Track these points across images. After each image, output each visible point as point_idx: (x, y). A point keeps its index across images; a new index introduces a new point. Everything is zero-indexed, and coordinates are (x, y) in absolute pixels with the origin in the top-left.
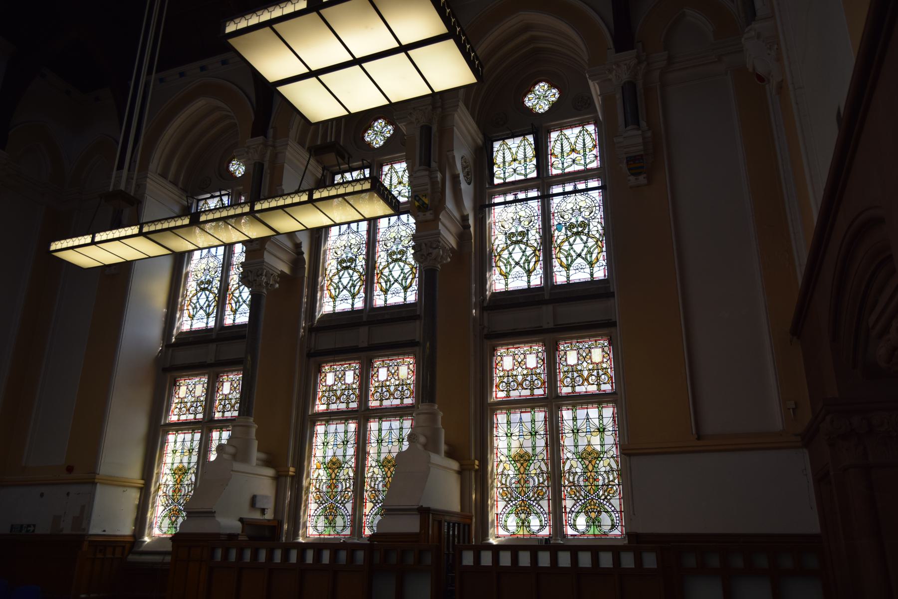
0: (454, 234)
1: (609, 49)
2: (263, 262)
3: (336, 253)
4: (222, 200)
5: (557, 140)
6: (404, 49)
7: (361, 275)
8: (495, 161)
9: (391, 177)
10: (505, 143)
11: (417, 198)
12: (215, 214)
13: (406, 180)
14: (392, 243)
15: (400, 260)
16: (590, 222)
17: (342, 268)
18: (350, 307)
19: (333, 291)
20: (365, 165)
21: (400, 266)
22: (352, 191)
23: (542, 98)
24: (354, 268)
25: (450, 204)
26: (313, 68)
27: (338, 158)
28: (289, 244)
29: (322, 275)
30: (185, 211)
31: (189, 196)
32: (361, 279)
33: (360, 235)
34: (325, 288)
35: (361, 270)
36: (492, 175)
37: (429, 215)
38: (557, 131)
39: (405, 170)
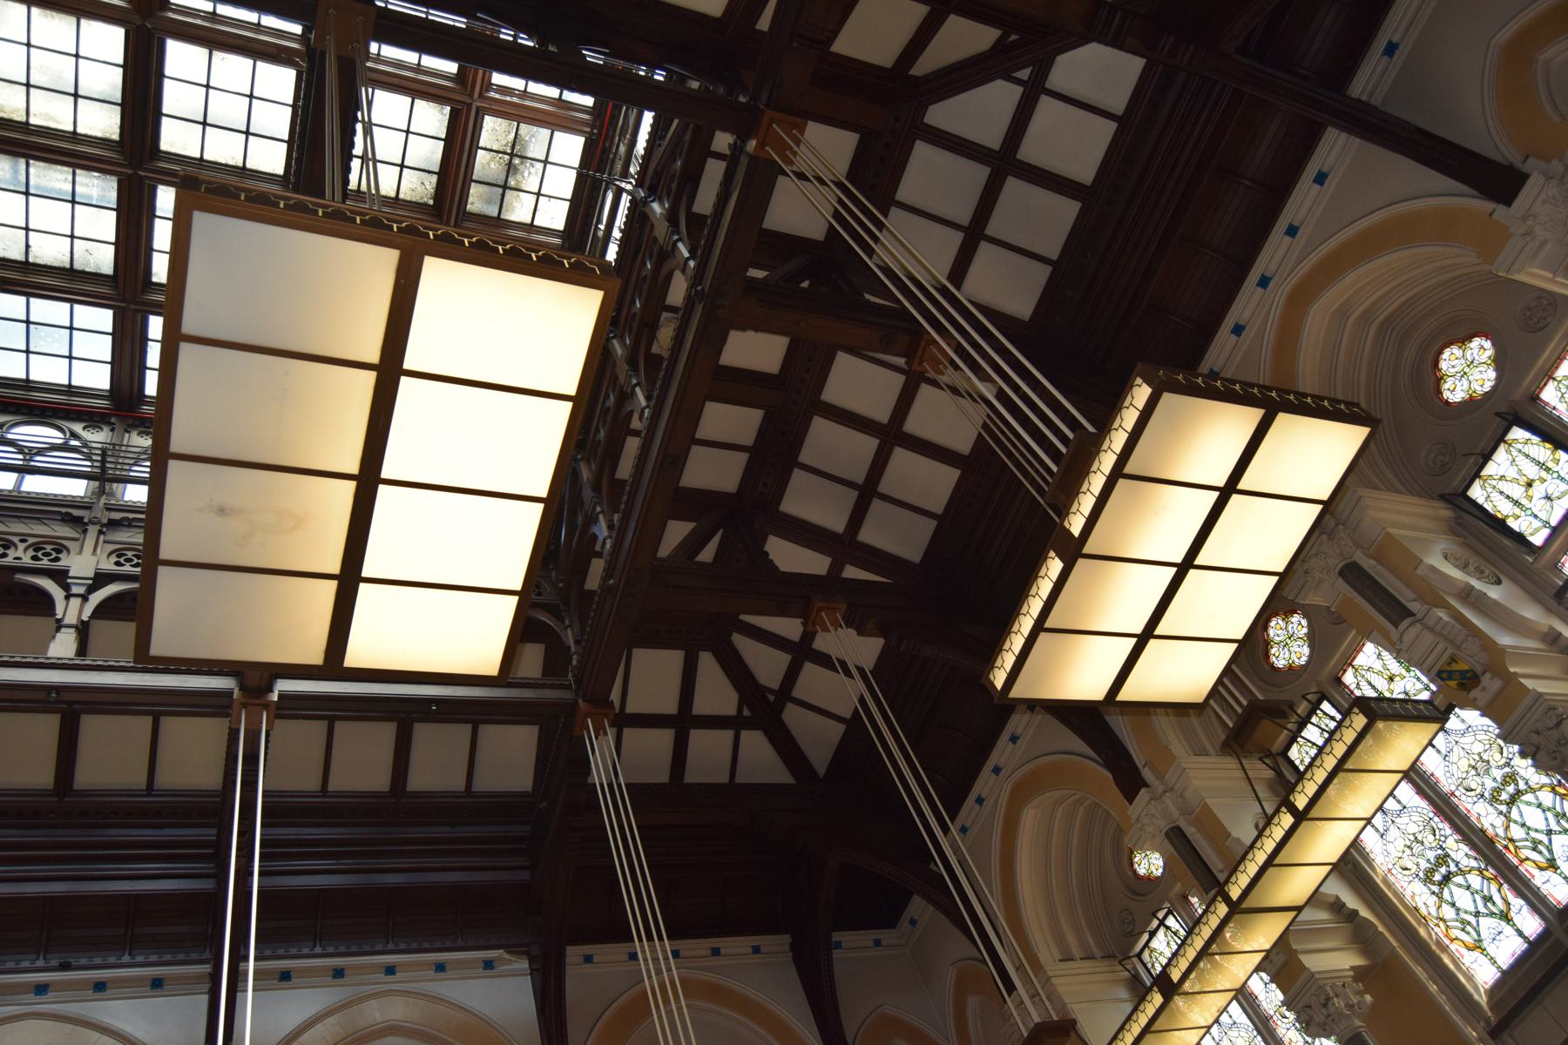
0: (1562, 676)
1: (1491, 214)
2: (1312, 975)
3: (1406, 869)
4: (1168, 928)
5: (1562, 396)
6: (1228, 491)
7: (1481, 872)
8: (1500, 516)
9: (1370, 684)
10: (1485, 478)
11: (1444, 675)
12: (1238, 882)
13: (1394, 666)
14: (1476, 778)
15: (1519, 793)
16: (1444, 849)
17: (1439, 885)
18: (1520, 940)
19: (1462, 936)
20: (1313, 701)
21: (1528, 804)
22: (1355, 735)
23: (1467, 370)
24: (1460, 869)
25: (1505, 640)
26: (1138, 630)
27: (1276, 720)
28: (1320, 915)
29: (1419, 923)
30: (1140, 994)
31: (1123, 960)
32: (1488, 879)
33: (1414, 809)
34: (1447, 942)
35: (1474, 863)
36: (1520, 538)
37: (1490, 684)
38: (1545, 385)
39: (1380, 654)
